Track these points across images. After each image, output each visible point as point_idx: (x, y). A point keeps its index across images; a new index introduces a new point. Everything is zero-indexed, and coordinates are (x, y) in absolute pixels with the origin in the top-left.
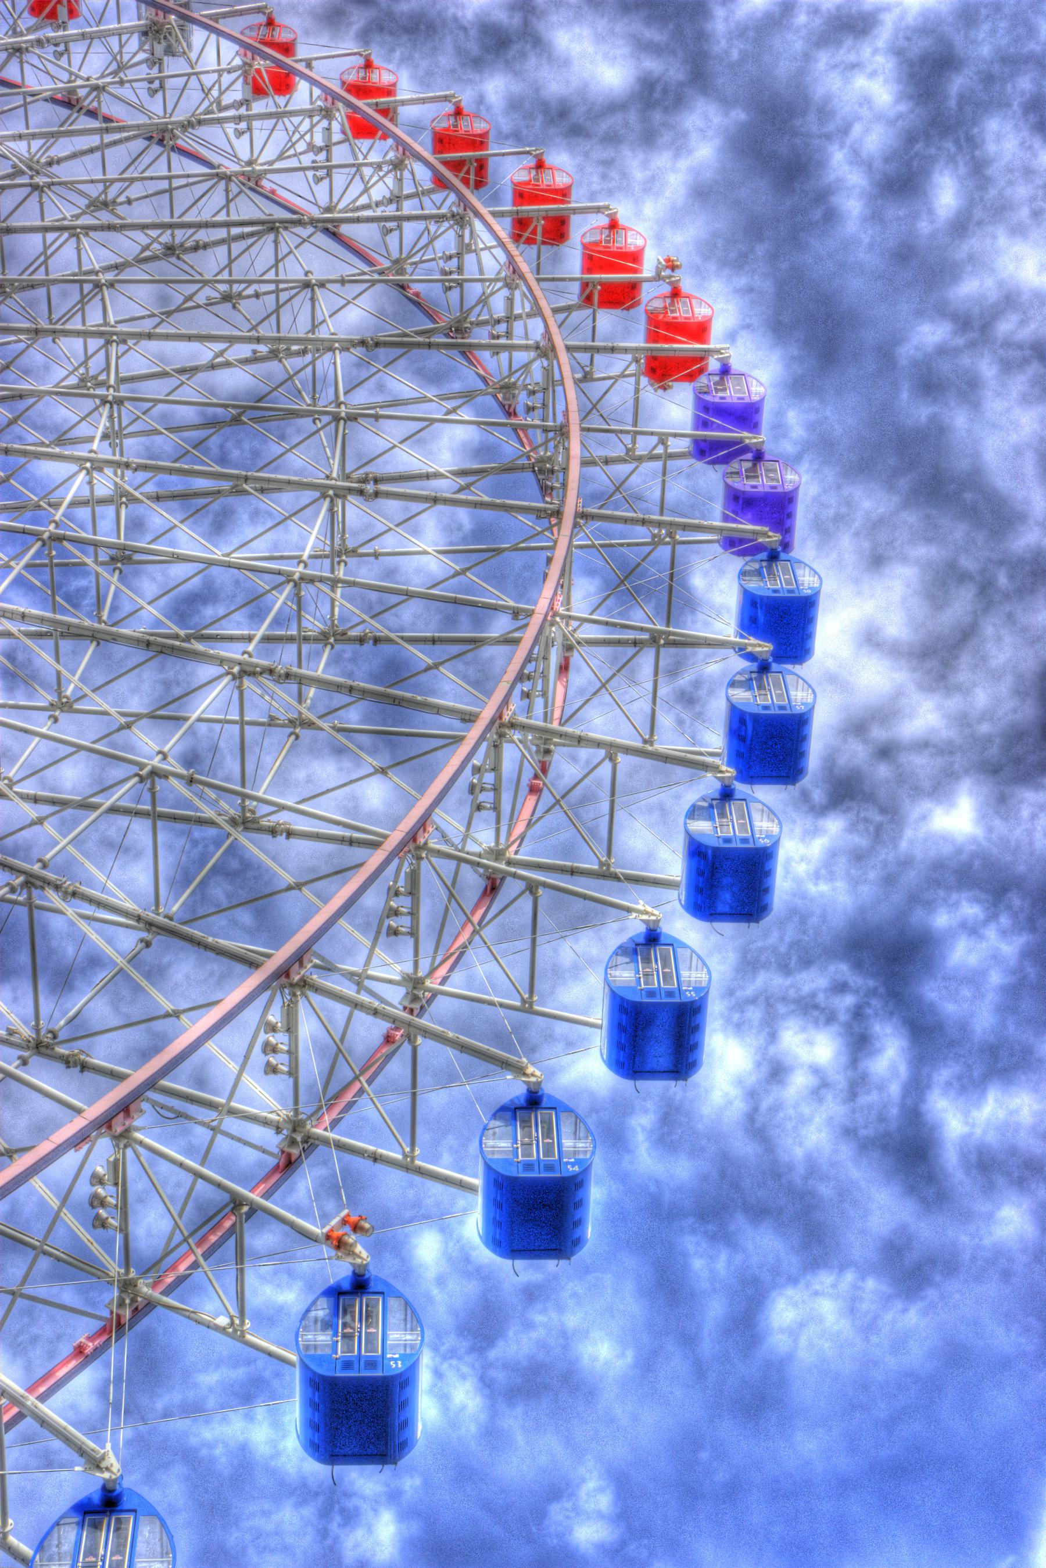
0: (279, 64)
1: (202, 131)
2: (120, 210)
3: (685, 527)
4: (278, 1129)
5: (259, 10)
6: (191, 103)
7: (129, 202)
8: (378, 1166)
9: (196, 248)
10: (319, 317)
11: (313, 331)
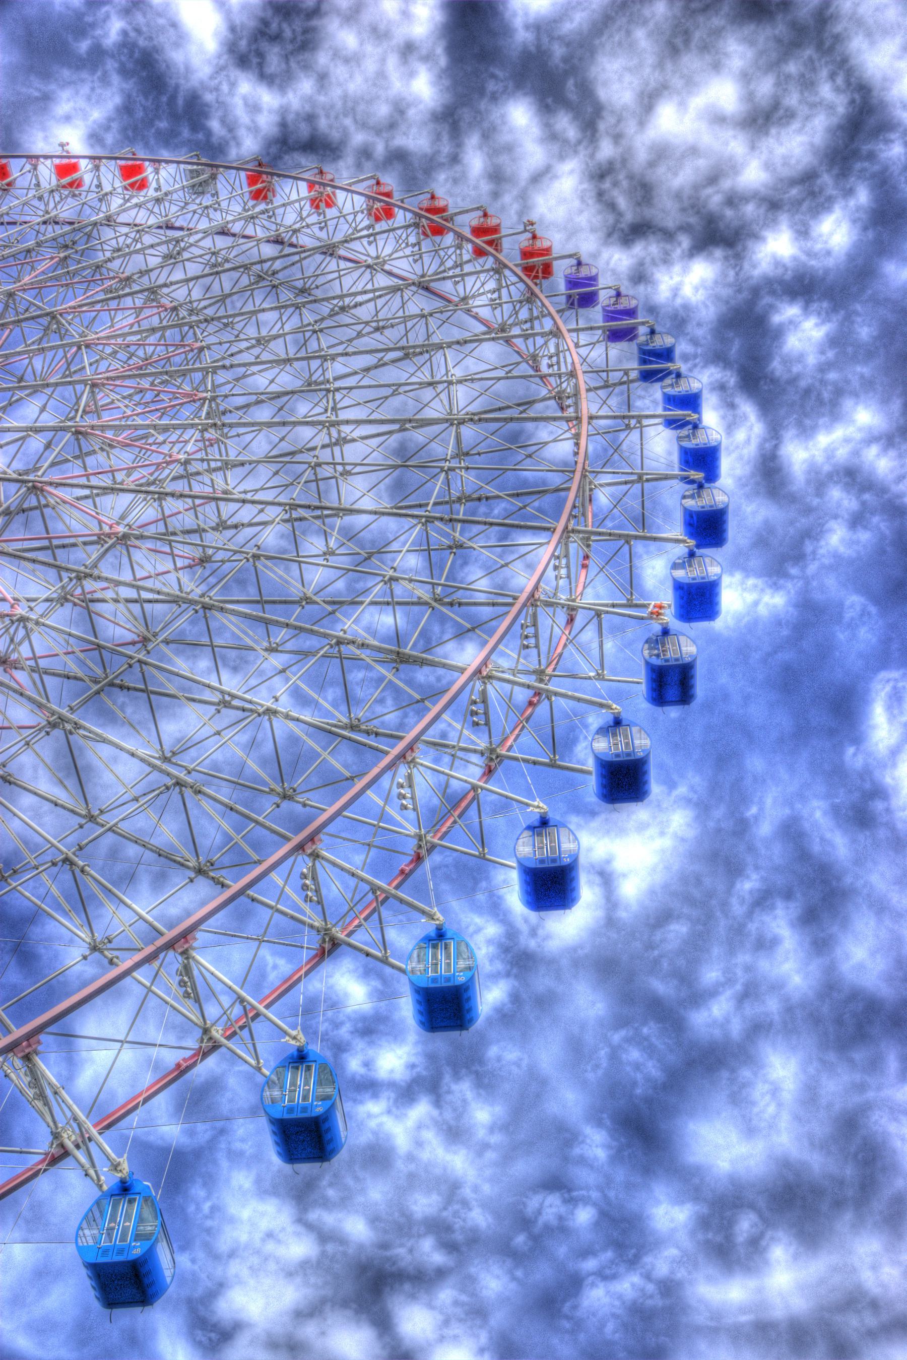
0: (387, 203)
1: (352, 245)
2: (313, 292)
3: (647, 417)
4: (482, 754)
5: (478, 209)
6: (344, 230)
7: (317, 287)
8: (255, 904)
9: (355, 306)
10: (431, 331)
11: (428, 339)
